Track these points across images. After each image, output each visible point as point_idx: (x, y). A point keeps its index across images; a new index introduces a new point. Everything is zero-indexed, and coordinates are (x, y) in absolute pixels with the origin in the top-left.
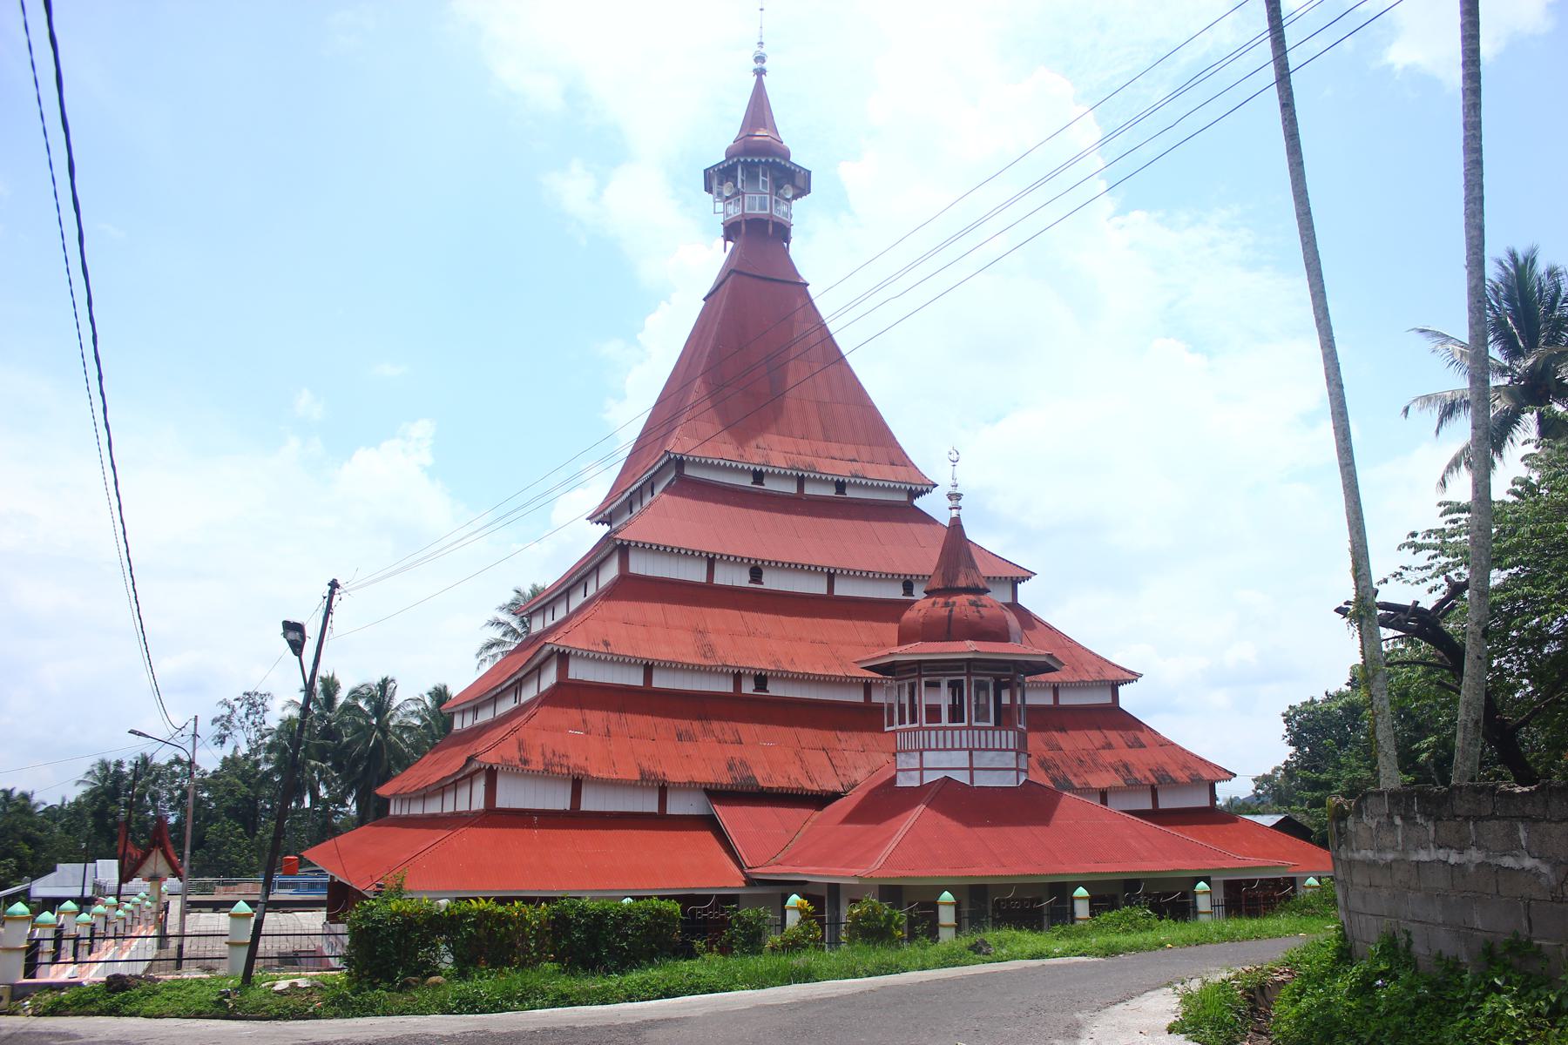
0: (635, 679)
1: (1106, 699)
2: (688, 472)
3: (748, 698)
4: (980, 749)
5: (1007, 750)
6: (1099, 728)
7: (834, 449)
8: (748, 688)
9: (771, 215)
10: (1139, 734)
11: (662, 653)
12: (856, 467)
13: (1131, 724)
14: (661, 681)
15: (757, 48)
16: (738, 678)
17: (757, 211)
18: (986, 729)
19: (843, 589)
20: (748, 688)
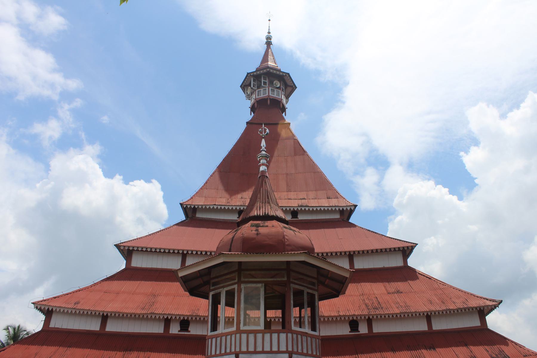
0: (94, 326)
1: (475, 322)
2: (199, 215)
3: (175, 337)
4: (248, 352)
5: (279, 352)
6: (466, 345)
7: (292, 195)
8: (175, 329)
9: (269, 96)
10: (503, 347)
11: (110, 307)
12: (300, 202)
13: (499, 340)
14: (112, 327)
15: (267, 34)
16: (167, 322)
17: (262, 96)
18: (255, 332)
19: (438, 325)
20: (175, 329)
